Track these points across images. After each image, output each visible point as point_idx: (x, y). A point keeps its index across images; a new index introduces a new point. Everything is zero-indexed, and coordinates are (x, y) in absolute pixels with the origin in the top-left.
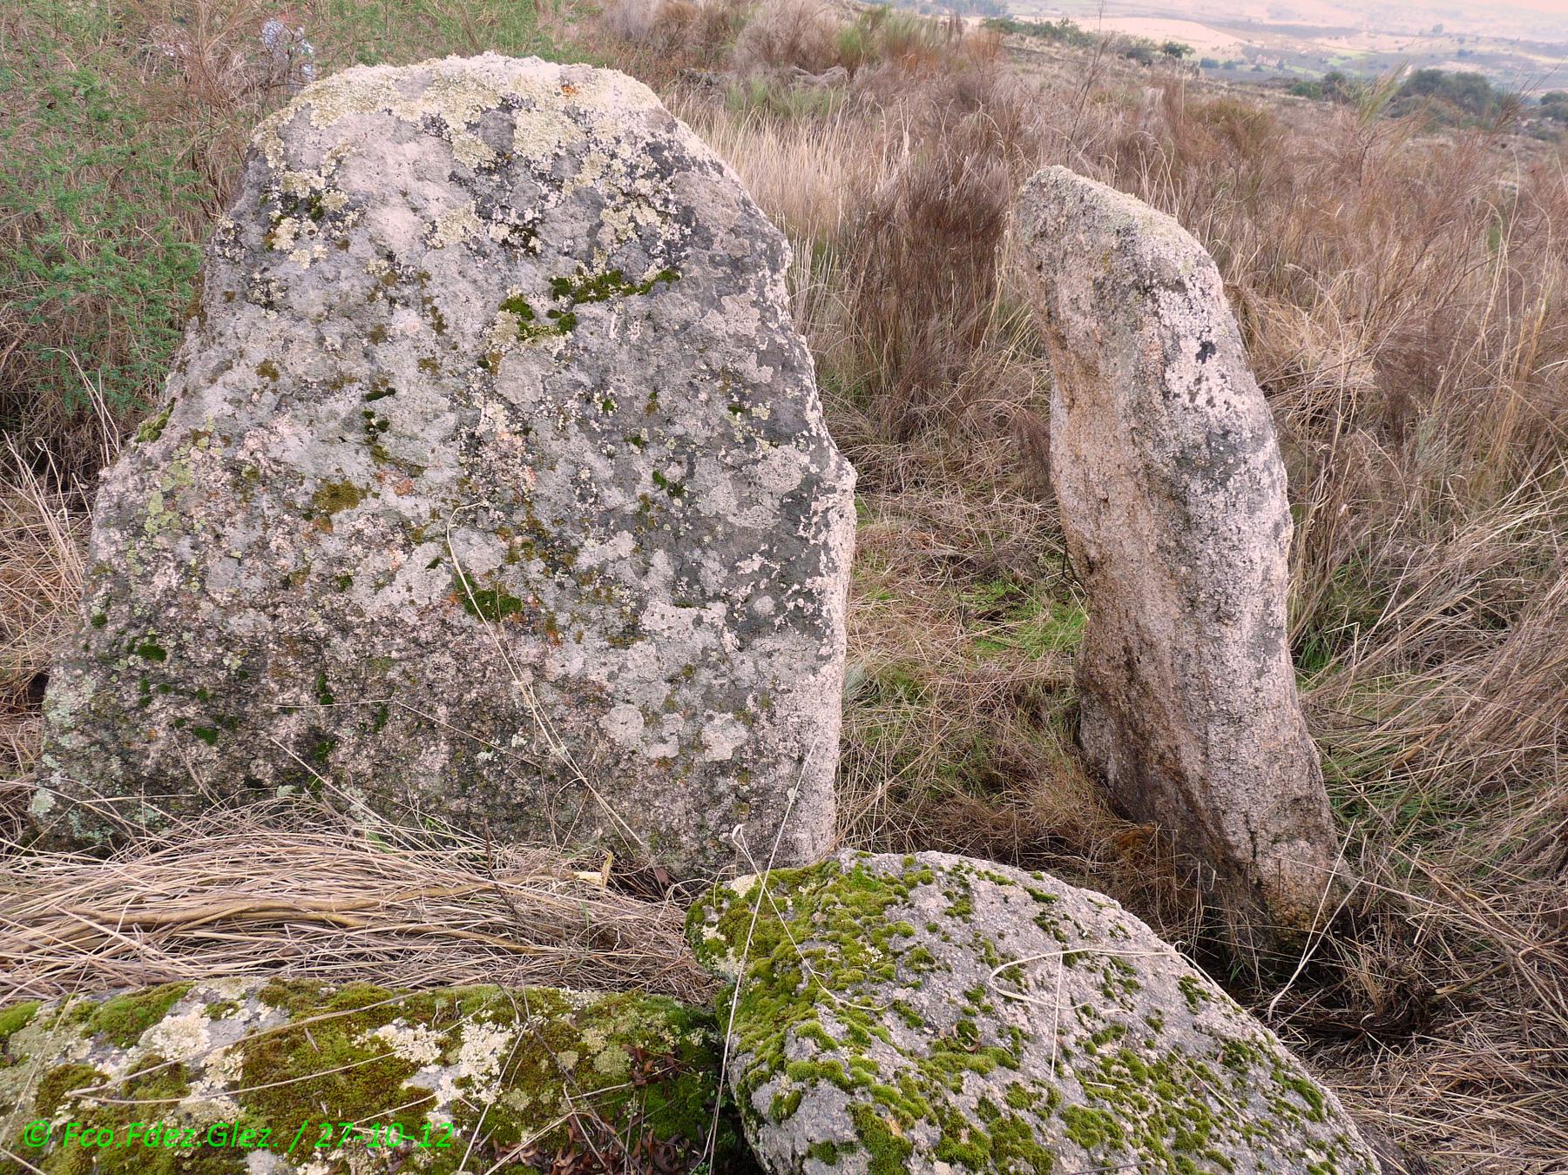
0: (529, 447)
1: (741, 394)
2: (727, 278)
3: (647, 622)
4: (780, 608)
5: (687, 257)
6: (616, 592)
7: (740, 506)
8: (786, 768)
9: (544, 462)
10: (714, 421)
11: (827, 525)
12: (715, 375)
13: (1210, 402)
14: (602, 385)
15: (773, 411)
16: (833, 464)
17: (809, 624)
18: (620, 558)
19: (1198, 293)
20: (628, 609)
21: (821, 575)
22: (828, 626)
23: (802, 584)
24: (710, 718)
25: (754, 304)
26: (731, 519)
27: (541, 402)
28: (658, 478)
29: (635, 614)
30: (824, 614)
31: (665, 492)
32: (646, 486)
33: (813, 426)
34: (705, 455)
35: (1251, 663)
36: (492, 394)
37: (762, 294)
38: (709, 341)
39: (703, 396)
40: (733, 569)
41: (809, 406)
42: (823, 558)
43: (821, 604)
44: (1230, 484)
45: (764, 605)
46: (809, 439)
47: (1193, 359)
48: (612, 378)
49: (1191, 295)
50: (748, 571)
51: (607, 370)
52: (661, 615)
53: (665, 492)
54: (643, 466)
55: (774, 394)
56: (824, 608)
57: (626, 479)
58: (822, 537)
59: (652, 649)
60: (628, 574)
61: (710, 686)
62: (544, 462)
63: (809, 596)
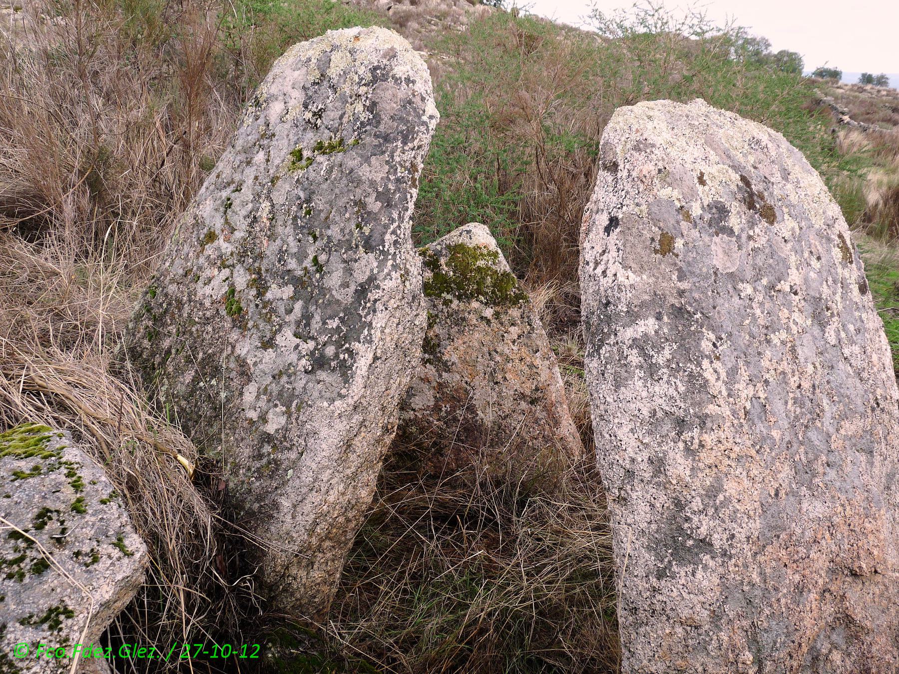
0: (272, 227)
1: (364, 215)
2: (380, 145)
3: (279, 339)
4: (337, 355)
5: (366, 131)
6: (273, 317)
7: (341, 286)
8: (293, 455)
9: (272, 237)
10: (347, 231)
11: (375, 311)
12: (356, 204)
13: (604, 272)
14: (308, 201)
15: (372, 230)
16: (386, 271)
17: (345, 370)
18: (282, 299)
19: (625, 173)
20: (274, 329)
21: (359, 342)
22: (352, 377)
23: (350, 344)
24: (276, 406)
25: (387, 162)
26: (334, 292)
27: (284, 205)
28: (315, 259)
29: (275, 333)
30: (354, 368)
31: (314, 268)
32: (308, 263)
33: (387, 245)
34: (336, 251)
35: (649, 558)
36: (269, 198)
37: (392, 157)
38: (359, 182)
39: (347, 215)
40: (324, 323)
41: (390, 231)
42: (366, 332)
43: (355, 362)
44: (602, 351)
45: (330, 351)
46: (382, 252)
47: (601, 231)
48: (315, 197)
49: (619, 175)
50: (330, 327)
51: (314, 193)
52: (286, 339)
53: (314, 268)
54: (311, 252)
55: (376, 220)
56: (355, 365)
57: (301, 256)
58: (369, 318)
59: (274, 355)
60: (282, 310)
61: (283, 387)
62: (272, 237)
63: (350, 352)
